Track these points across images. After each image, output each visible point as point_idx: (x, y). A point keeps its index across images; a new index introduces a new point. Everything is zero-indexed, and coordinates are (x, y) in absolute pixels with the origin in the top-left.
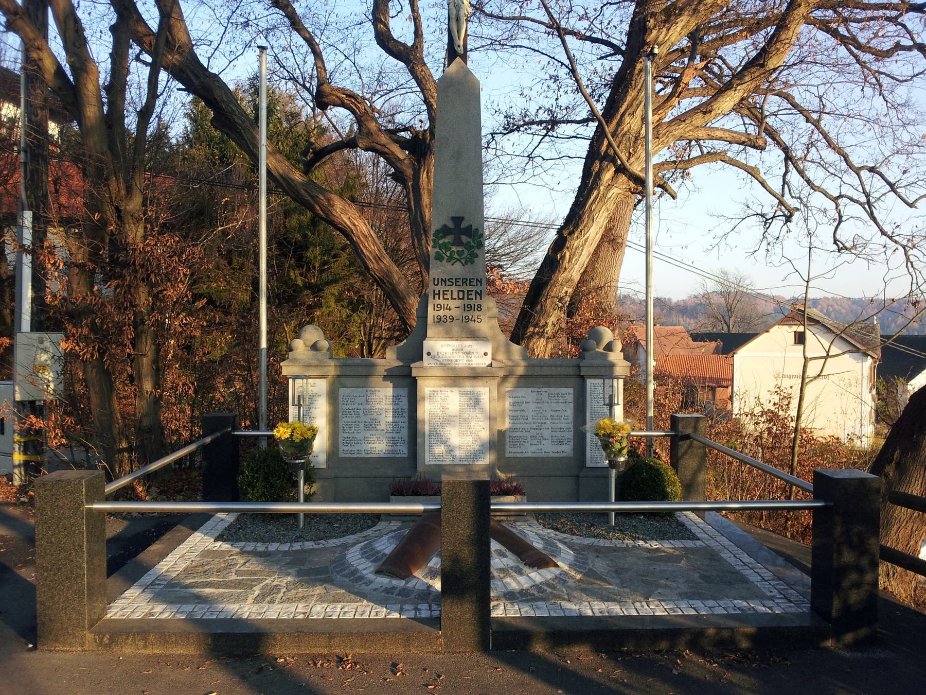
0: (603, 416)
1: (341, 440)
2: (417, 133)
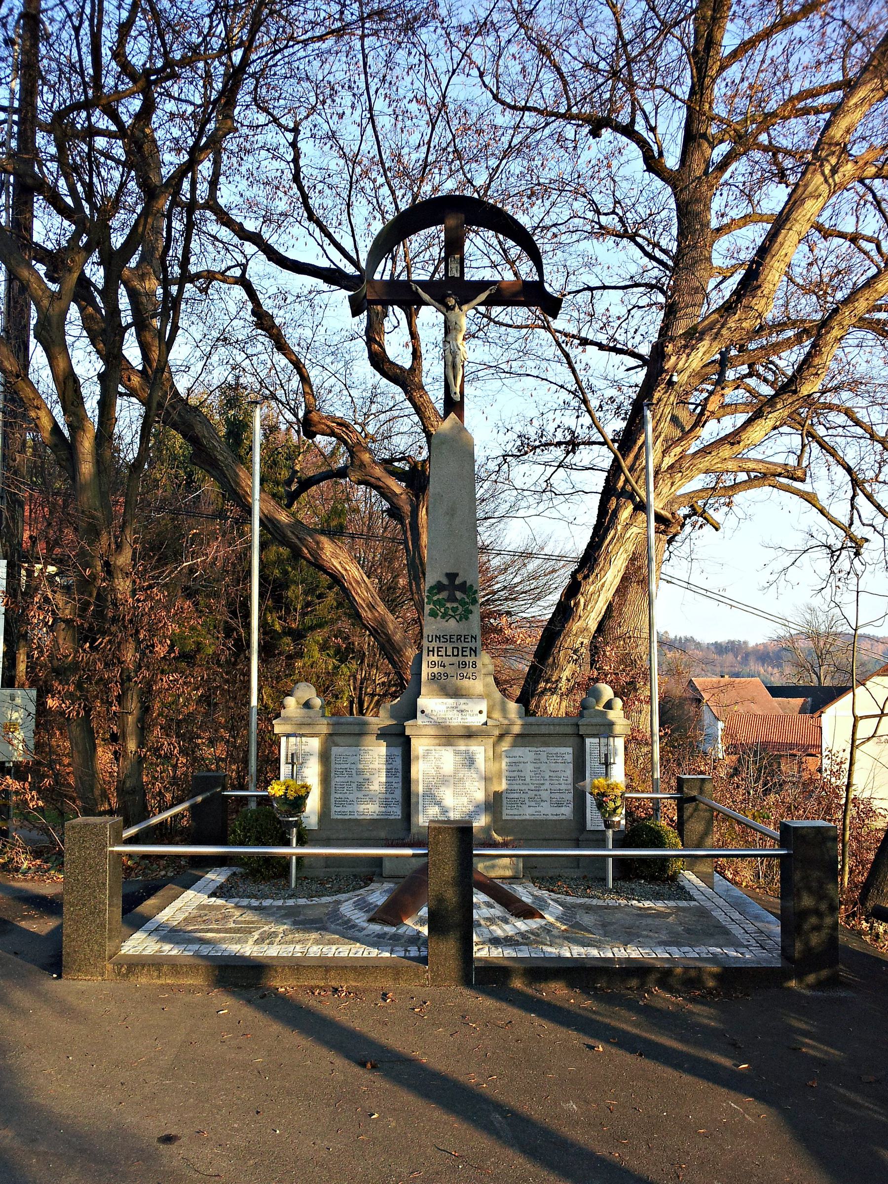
0: (595, 775)
1: (333, 800)
2: (416, 463)
